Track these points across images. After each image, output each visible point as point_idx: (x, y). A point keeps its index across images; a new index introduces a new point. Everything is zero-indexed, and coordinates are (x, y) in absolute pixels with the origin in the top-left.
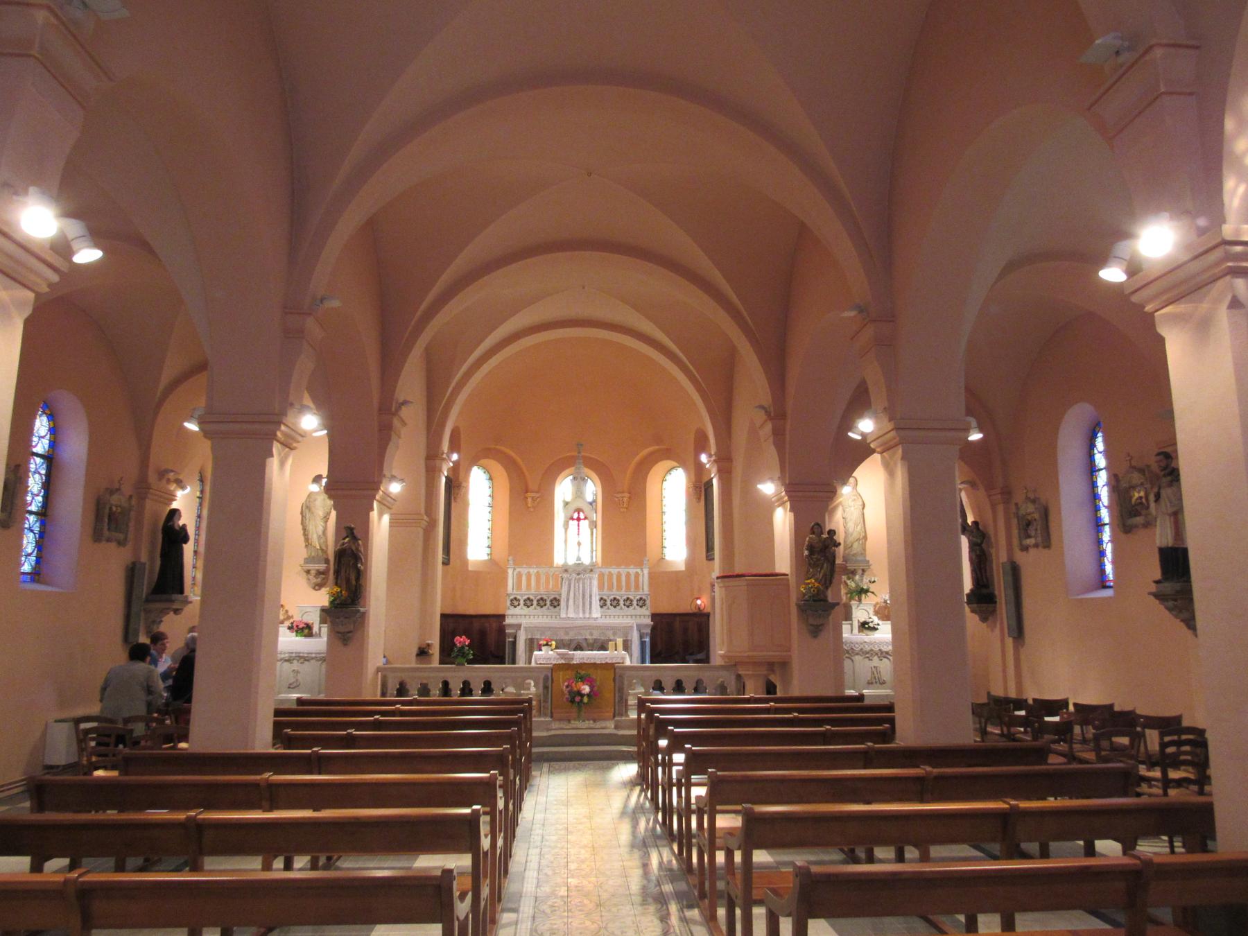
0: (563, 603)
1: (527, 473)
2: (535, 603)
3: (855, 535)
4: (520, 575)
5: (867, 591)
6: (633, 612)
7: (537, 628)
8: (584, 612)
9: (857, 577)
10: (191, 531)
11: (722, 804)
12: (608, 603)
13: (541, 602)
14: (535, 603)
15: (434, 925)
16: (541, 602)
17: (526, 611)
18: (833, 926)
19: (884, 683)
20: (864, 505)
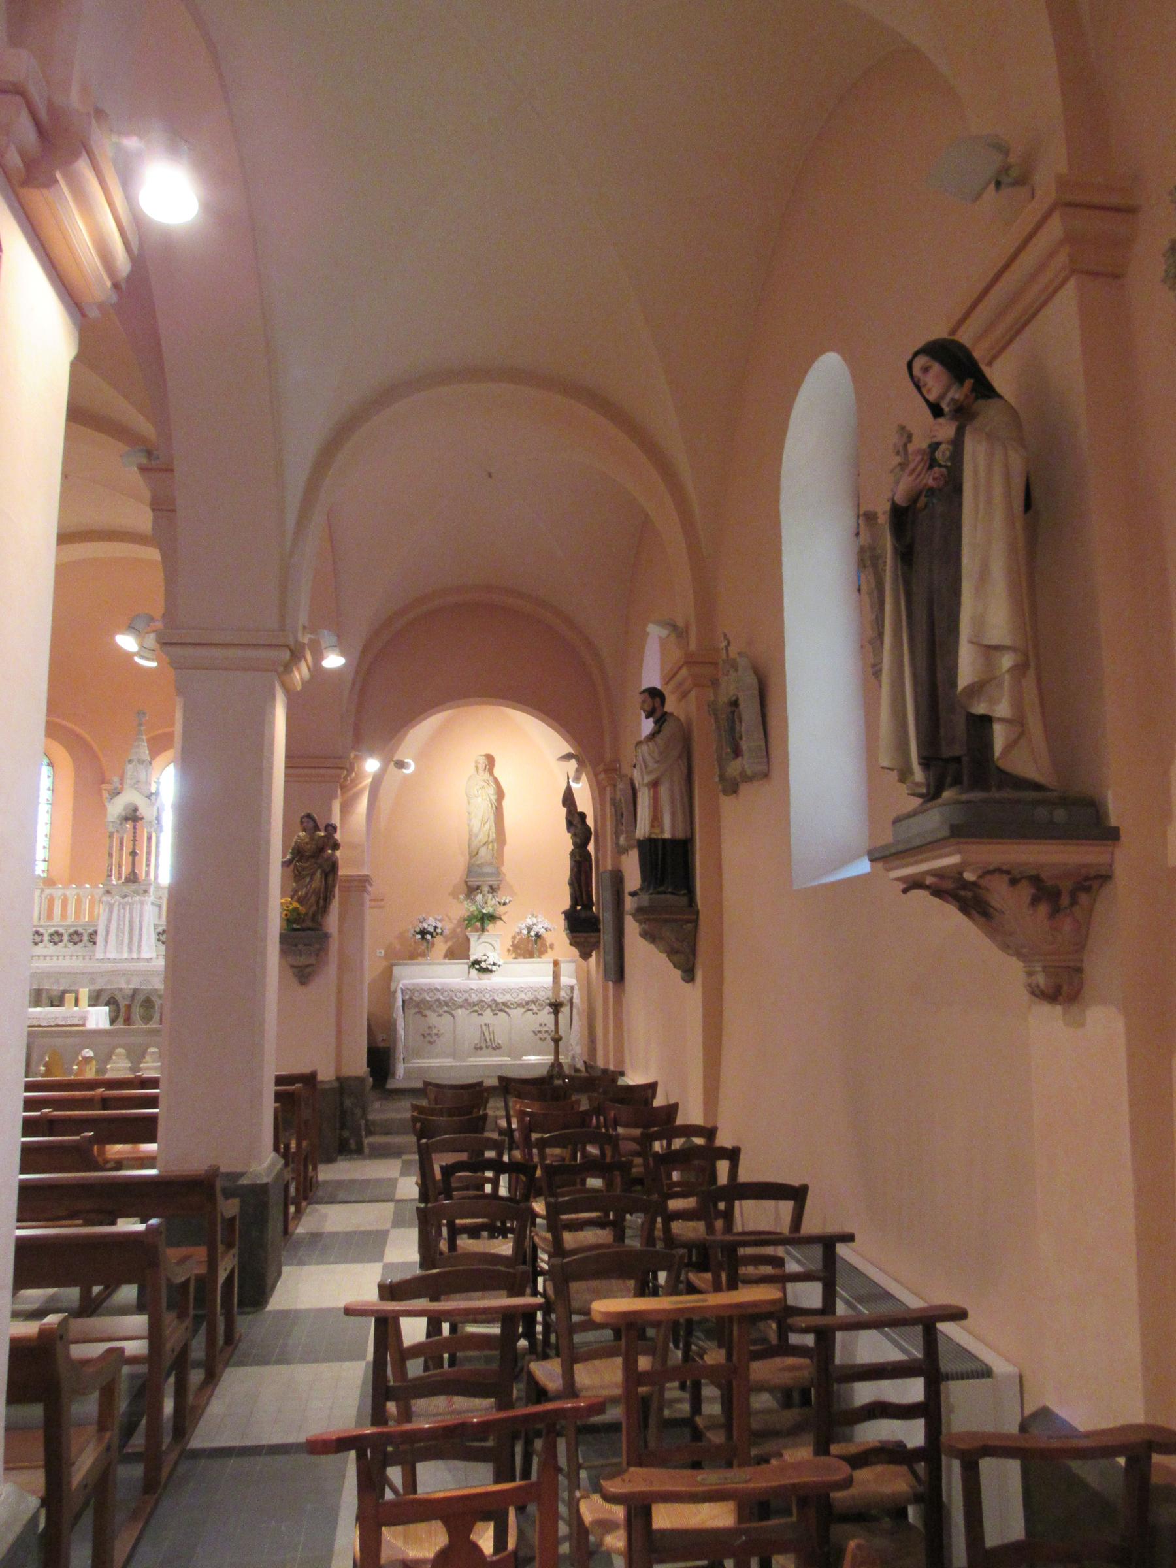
0: (100, 939)
1: (100, 755)
2: (66, 938)
3: (482, 837)
4: (51, 901)
5: (492, 918)
6: (46, 952)
7: (47, 975)
8: (130, 950)
9: (479, 897)
10: (338, 825)
11: (462, 1218)
12: (85, 938)
13: (76, 937)
14: (66, 938)
15: (917, 1421)
16: (76, 937)
17: (51, 949)
18: (241, 1363)
19: (498, 1047)
20: (500, 794)
